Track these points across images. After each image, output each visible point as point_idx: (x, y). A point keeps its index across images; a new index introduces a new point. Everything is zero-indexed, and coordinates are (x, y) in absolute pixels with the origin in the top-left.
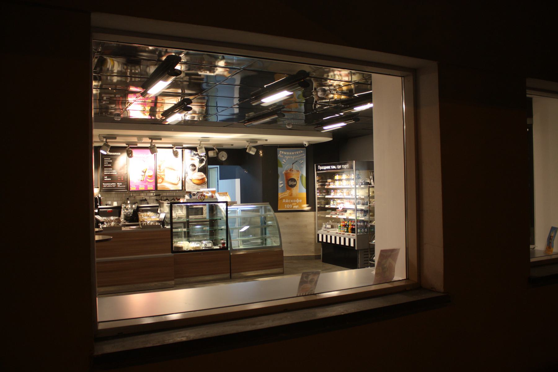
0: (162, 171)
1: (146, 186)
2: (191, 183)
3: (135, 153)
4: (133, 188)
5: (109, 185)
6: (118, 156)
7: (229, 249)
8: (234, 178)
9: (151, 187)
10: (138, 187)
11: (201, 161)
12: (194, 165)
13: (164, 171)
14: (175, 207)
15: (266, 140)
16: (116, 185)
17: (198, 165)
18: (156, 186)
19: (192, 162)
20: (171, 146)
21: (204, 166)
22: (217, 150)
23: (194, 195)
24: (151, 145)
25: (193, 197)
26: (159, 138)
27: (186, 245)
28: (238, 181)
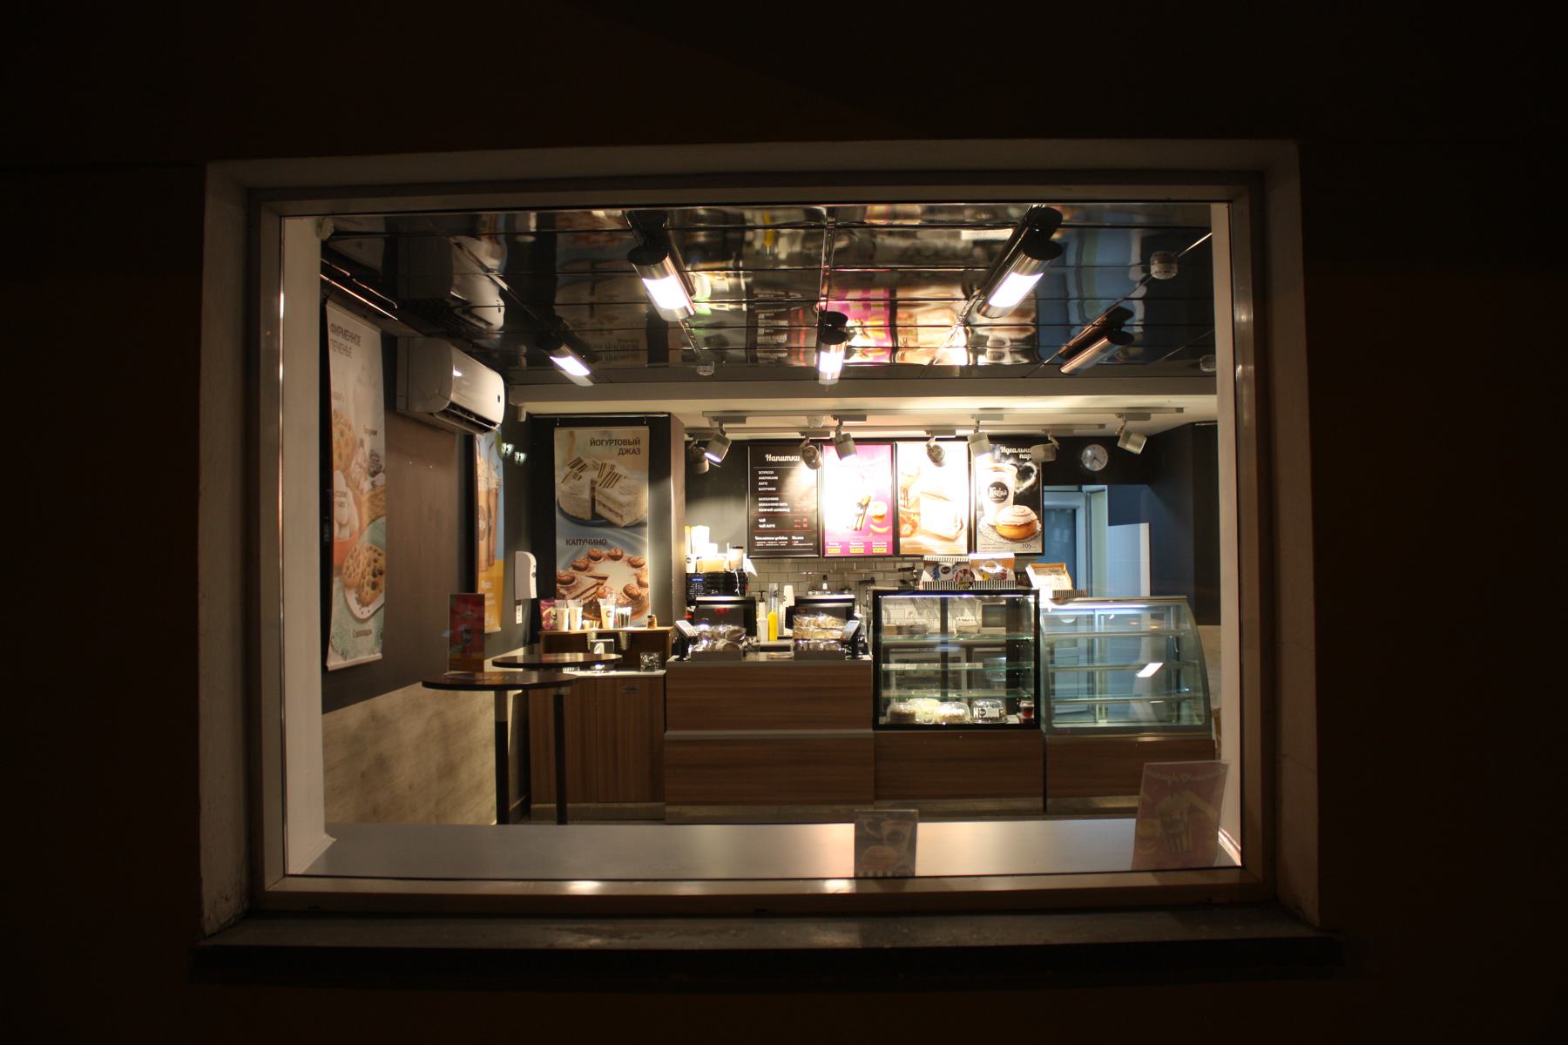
0: (912, 501)
1: (868, 545)
2: (995, 537)
3: (829, 456)
4: (833, 550)
5: (771, 541)
6: (793, 463)
7: (1043, 727)
8: (1138, 521)
9: (881, 548)
10: (845, 546)
11: (1024, 474)
12: (1000, 486)
13: (917, 502)
14: (954, 601)
15: (1180, 410)
16: (790, 540)
17: (1014, 485)
18: (896, 545)
19: (996, 477)
20: (922, 434)
21: (1031, 487)
22: (1055, 443)
23: (946, 570)
24: (838, 434)
25: (943, 577)
26: (859, 415)
27: (928, 708)
28: (1144, 529)
